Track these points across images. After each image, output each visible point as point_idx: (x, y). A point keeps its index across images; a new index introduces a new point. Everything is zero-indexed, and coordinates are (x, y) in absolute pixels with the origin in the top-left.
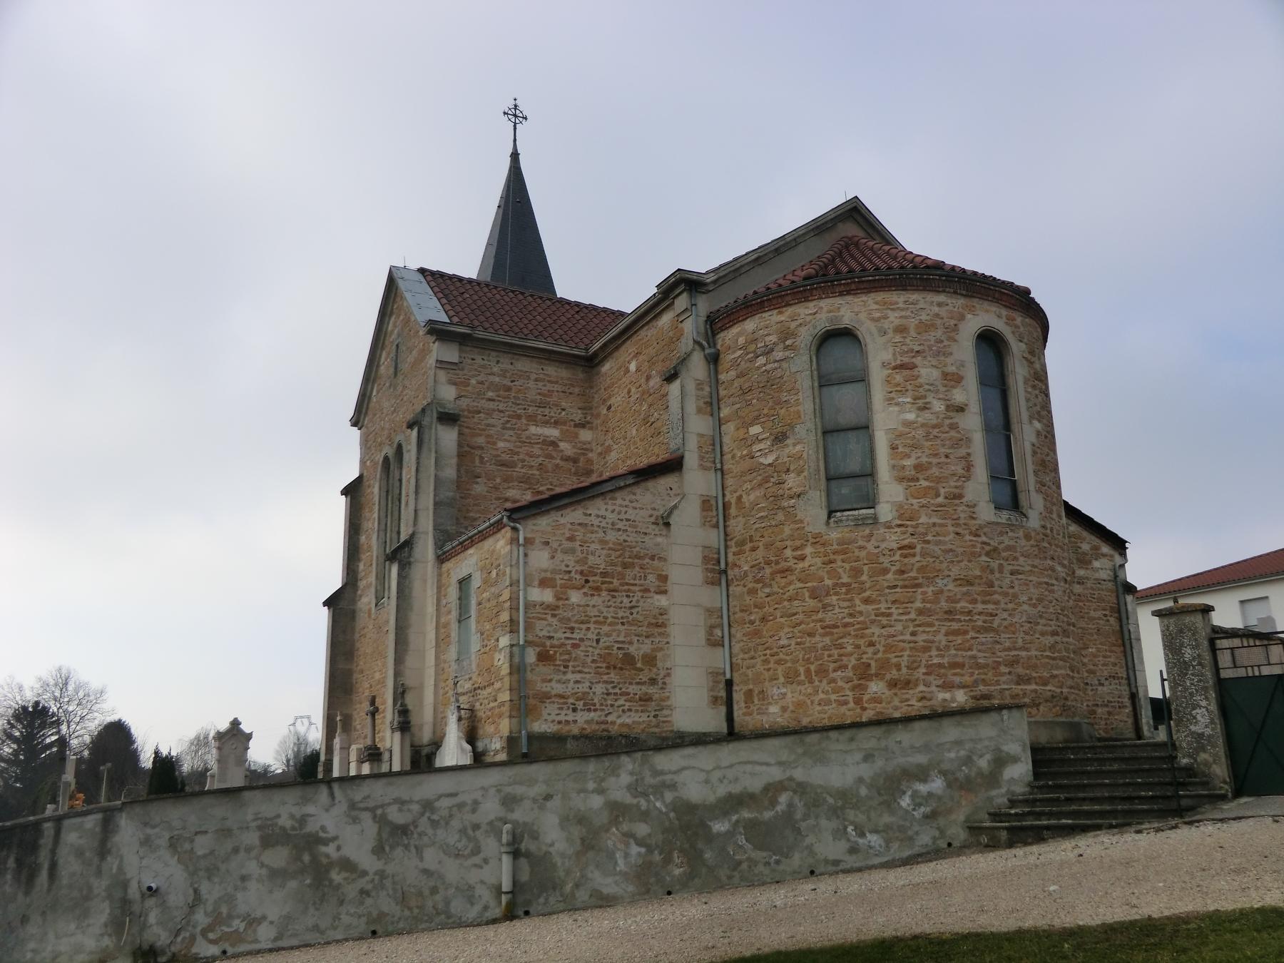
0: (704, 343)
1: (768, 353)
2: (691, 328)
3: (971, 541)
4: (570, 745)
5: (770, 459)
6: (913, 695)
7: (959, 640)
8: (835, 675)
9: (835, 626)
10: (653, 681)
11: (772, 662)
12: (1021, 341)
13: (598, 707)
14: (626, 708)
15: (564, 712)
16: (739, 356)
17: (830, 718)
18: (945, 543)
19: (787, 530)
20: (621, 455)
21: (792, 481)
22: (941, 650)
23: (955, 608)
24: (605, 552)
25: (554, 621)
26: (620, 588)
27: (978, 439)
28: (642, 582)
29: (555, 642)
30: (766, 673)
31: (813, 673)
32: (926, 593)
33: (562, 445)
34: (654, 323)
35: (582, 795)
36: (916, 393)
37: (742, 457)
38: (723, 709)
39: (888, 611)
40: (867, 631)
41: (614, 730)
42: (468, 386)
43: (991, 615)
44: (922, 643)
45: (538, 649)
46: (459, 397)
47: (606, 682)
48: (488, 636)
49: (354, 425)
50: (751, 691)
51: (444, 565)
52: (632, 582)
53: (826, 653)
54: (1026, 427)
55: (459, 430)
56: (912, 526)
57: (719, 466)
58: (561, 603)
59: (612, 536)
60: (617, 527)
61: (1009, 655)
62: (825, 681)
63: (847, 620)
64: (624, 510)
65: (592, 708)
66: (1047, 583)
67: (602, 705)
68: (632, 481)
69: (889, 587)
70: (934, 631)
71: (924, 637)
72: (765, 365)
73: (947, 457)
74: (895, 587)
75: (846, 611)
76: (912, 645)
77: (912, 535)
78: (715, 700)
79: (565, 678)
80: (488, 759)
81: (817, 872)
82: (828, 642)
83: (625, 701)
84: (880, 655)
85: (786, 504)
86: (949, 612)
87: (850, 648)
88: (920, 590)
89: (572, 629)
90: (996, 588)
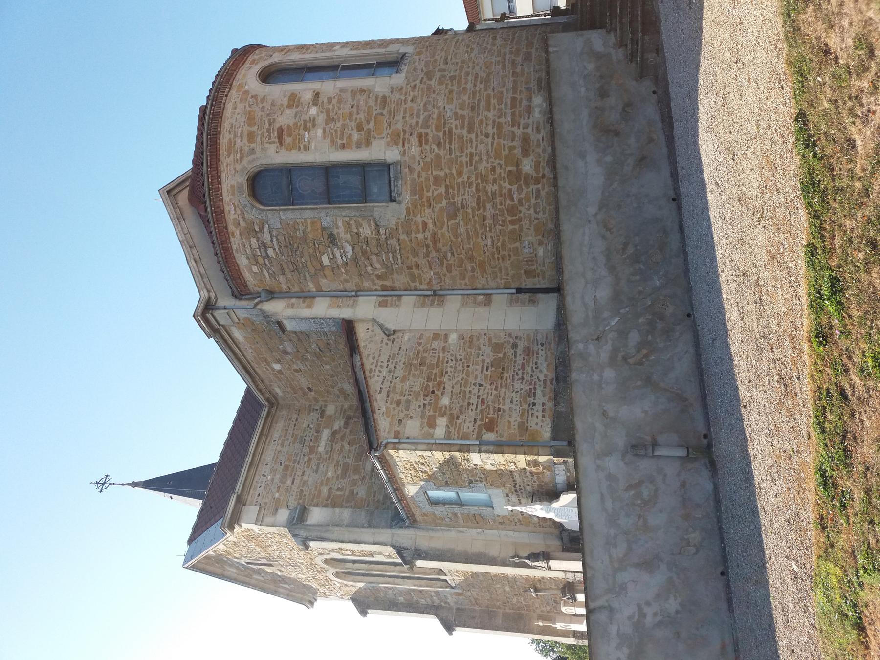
0: (256, 300)
1: (265, 246)
2: (243, 309)
3: (418, 91)
4: (562, 408)
5: (349, 249)
6: (534, 137)
7: (494, 101)
10: (515, 346)
11: (504, 253)
12: (271, 56)
13: (532, 387)
14: (534, 366)
15: (536, 413)
16: (268, 272)
17: (549, 204)
18: (419, 110)
20: (346, 379)
21: (366, 231)
22: (502, 114)
23: (469, 103)
24: (411, 378)
25: (462, 417)
26: (440, 367)
27: (342, 83)
28: (436, 351)
29: (479, 417)
30: (513, 258)
31: (514, 218)
32: (456, 126)
33: (336, 427)
34: (241, 346)
35: (604, 386)
36: (302, 128)
37: (347, 272)
38: (540, 296)
39: (469, 156)
40: (483, 173)
41: (551, 375)
42: (280, 499)
43: (476, 77)
44: (495, 130)
45: (484, 431)
46: (288, 507)
47: (513, 380)
48: (472, 476)
49: (312, 603)
50: (525, 272)
51: (418, 519)
52: (436, 359)
53: (499, 207)
54: (337, 53)
55: (314, 506)
56: (404, 134)
57: (353, 293)
58: (448, 412)
59: (399, 373)
60: (393, 369)
61: (508, 66)
62: (520, 208)
63: (474, 189)
64: (380, 363)
65: (533, 391)
66: (456, 42)
67: (531, 384)
68: (358, 357)
69: (450, 154)
70: (486, 120)
71: (490, 127)
72: (275, 249)
73: (352, 107)
74: (450, 149)
75: (467, 189)
76: (496, 137)
77: (411, 135)
78: (532, 302)
79: (508, 411)
80: (573, 479)
81: (674, 196)
82: (490, 204)
83: (529, 366)
84: (502, 162)
85: (384, 237)
86: (473, 108)
87: (496, 187)
88: (454, 130)
89: (469, 404)
90: (457, 74)
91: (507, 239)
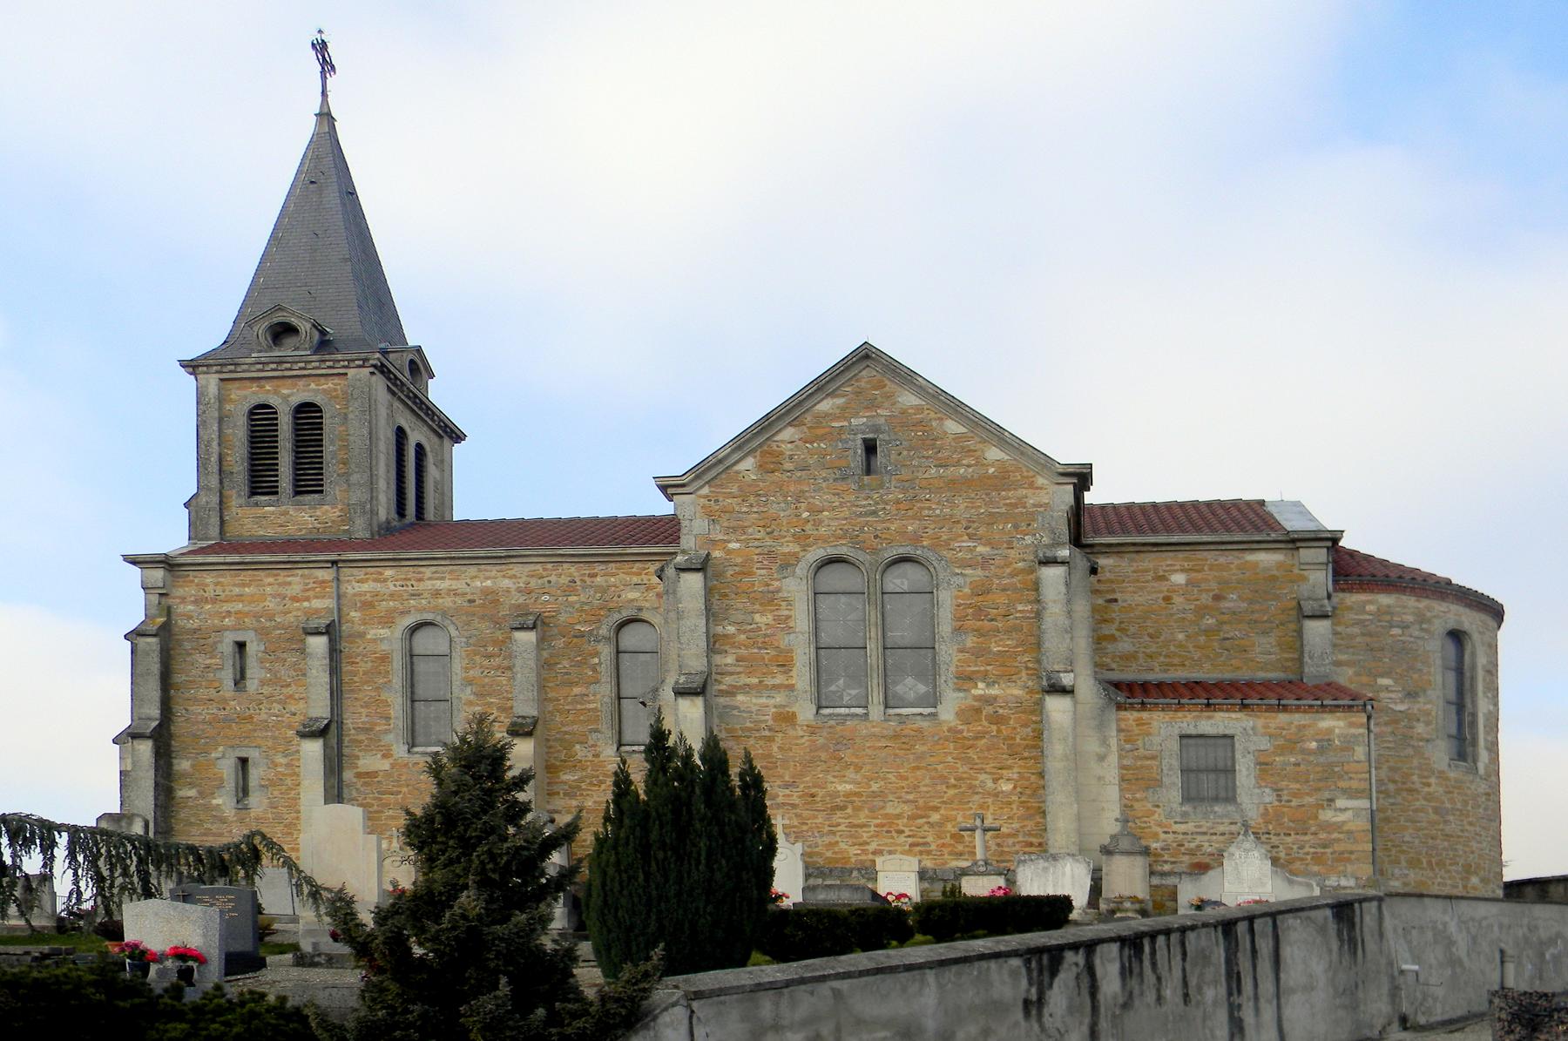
8: (1450, 868)
9: (1452, 836)
19: (1415, 762)
21: (1420, 728)
91: (1411, 855)
